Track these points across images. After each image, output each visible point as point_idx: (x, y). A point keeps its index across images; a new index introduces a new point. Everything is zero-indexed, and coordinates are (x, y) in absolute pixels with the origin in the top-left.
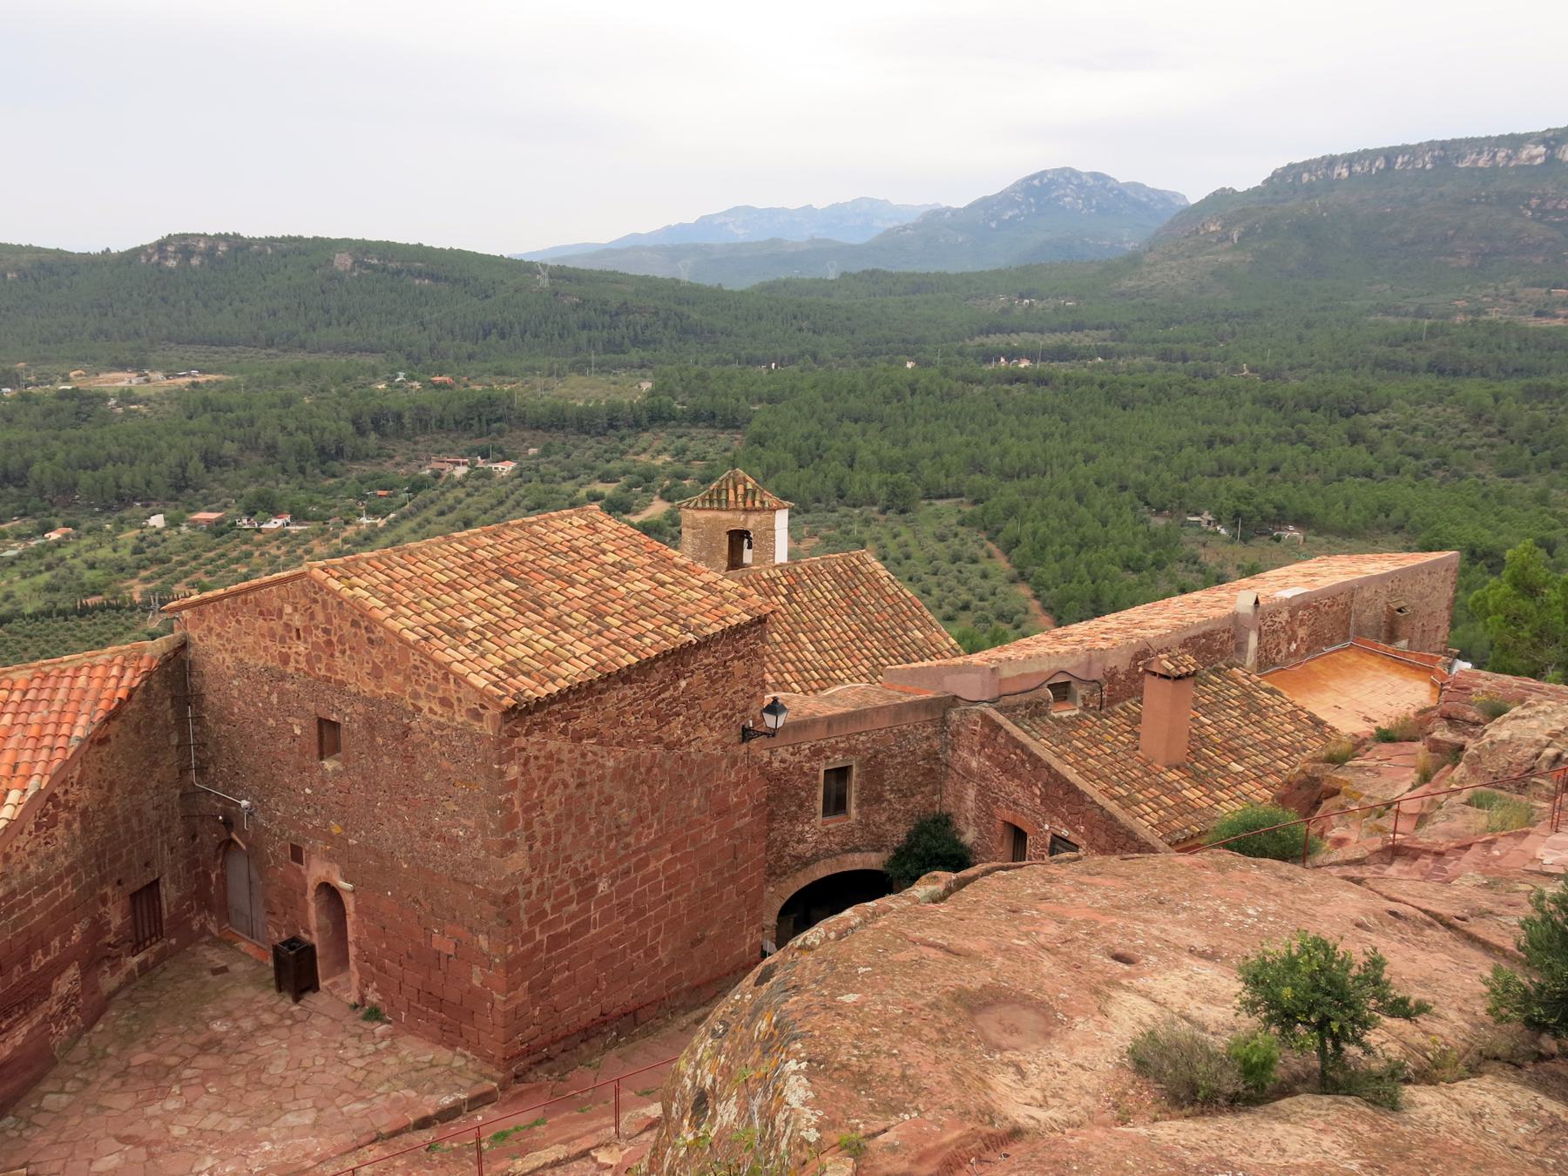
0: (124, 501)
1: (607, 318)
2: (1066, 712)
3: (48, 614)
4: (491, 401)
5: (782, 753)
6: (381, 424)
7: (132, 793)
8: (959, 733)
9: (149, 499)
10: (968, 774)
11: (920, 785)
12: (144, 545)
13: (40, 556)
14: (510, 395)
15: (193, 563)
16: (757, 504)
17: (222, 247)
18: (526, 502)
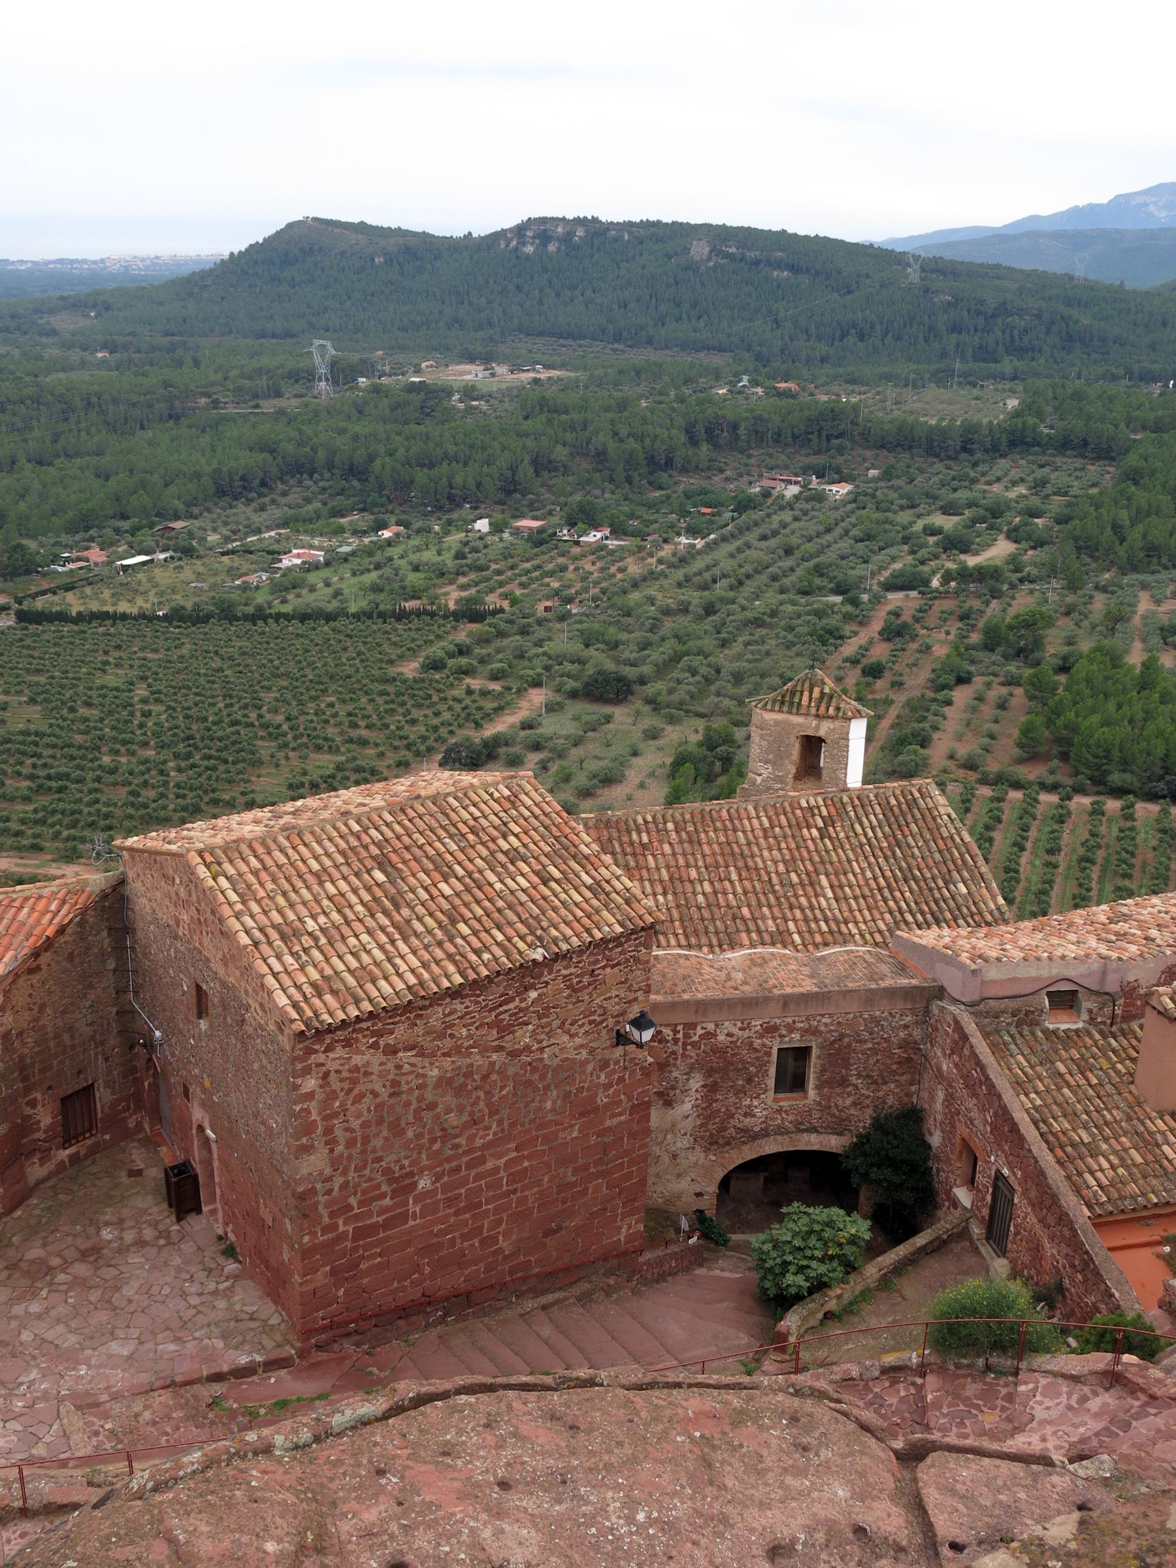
0: (455, 502)
1: (981, 321)
2: (1063, 1023)
3: (369, 615)
4: (833, 414)
6: (716, 434)
7: (64, 1012)
9: (476, 500)
11: (894, 1073)
12: (467, 550)
13: (371, 554)
14: (855, 408)
15: (509, 574)
16: (831, 711)
17: (580, 232)
18: (855, 532)
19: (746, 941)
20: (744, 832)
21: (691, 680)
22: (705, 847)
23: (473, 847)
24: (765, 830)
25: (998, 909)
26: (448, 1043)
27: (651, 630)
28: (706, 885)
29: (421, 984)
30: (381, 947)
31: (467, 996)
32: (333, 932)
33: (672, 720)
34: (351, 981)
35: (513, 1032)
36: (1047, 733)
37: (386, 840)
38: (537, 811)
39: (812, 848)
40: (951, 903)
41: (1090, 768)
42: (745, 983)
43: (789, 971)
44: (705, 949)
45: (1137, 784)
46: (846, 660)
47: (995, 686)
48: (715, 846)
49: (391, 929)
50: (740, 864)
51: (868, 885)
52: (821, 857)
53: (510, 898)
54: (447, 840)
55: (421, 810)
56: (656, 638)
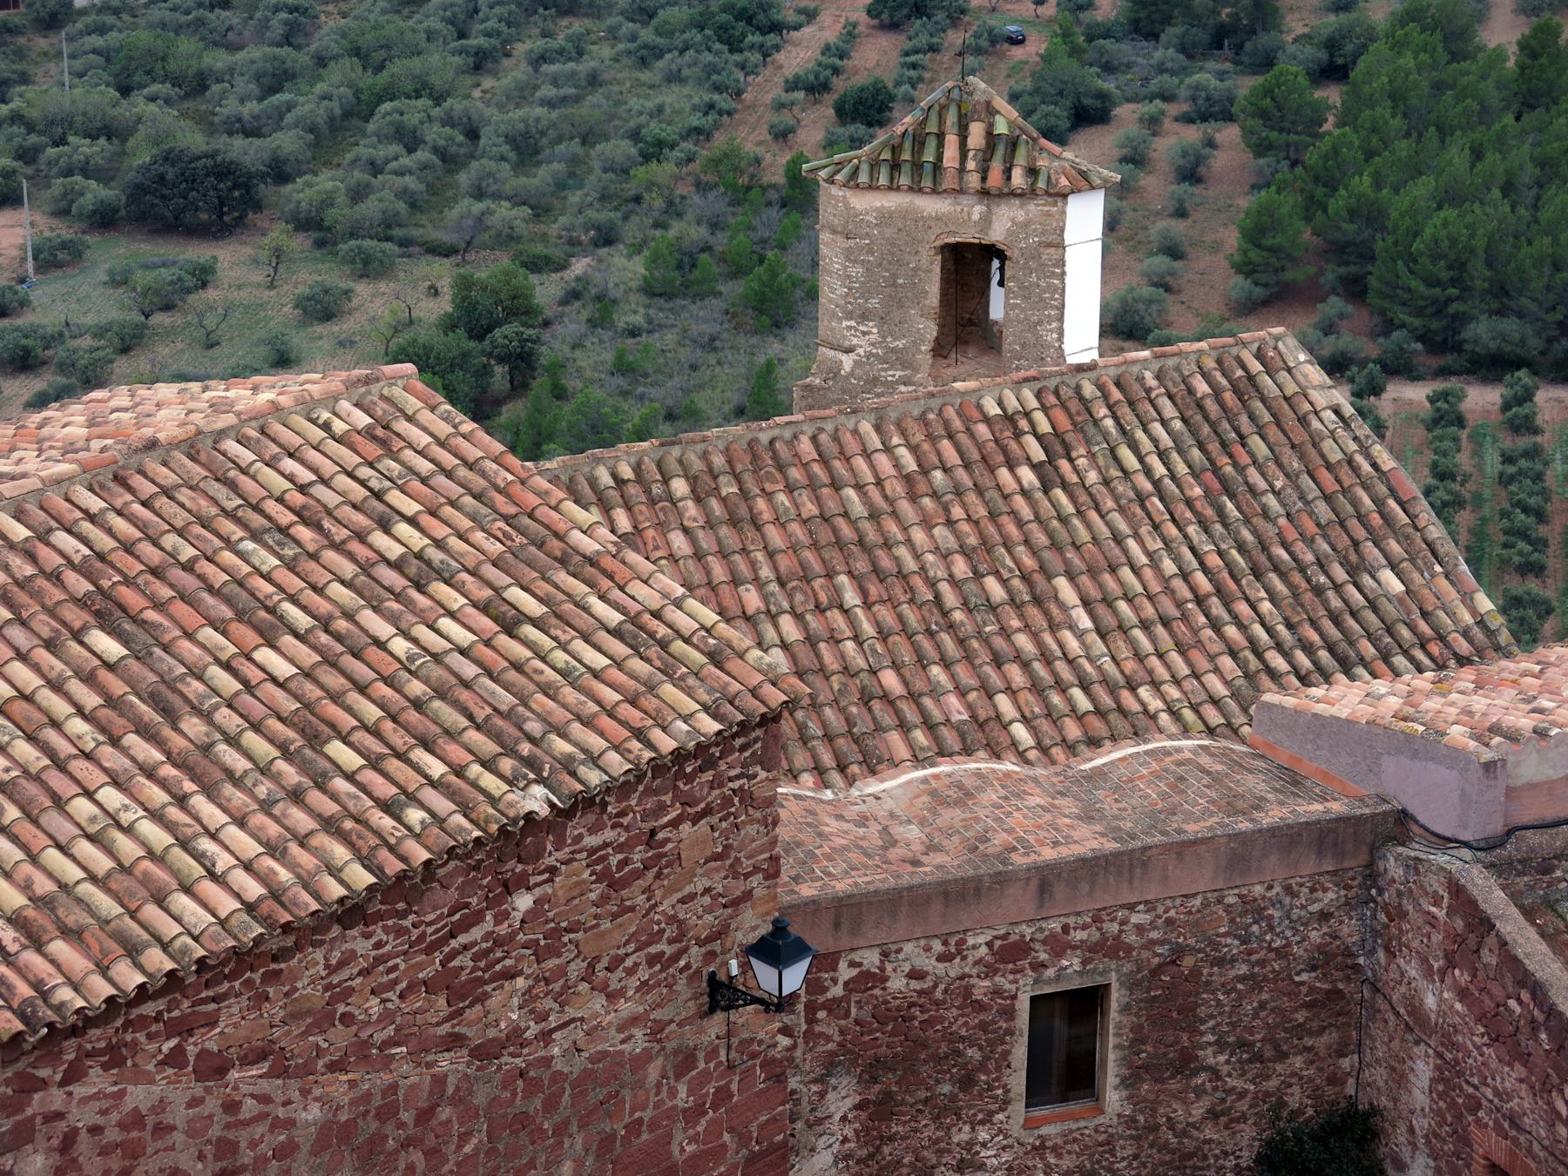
5: (913, 954)
8: (1403, 915)
10: (1416, 1022)
11: (1301, 1030)
16: (1018, 178)
19: (902, 752)
20: (859, 487)
21: (406, 161)
22: (772, 532)
23: (314, 557)
24: (908, 479)
25: (1481, 623)
26: (340, 1037)
27: (288, 39)
28: (786, 622)
29: (276, 893)
30: (156, 816)
31: (380, 916)
32: (32, 789)
33: (368, 268)
34: (106, 904)
35: (482, 998)
36: (1307, 235)
37: (101, 557)
38: (449, 460)
39: (1026, 513)
40: (1370, 616)
41: (1419, 312)
42: (931, 848)
43: (1033, 811)
44: (807, 779)
45: (1535, 344)
46: (793, 85)
47: (1168, 124)
48: (795, 527)
49: (168, 771)
50: (862, 566)
51: (1169, 591)
52: (1050, 535)
53: (437, 672)
54: (249, 545)
55: (167, 476)
56: (303, 59)
